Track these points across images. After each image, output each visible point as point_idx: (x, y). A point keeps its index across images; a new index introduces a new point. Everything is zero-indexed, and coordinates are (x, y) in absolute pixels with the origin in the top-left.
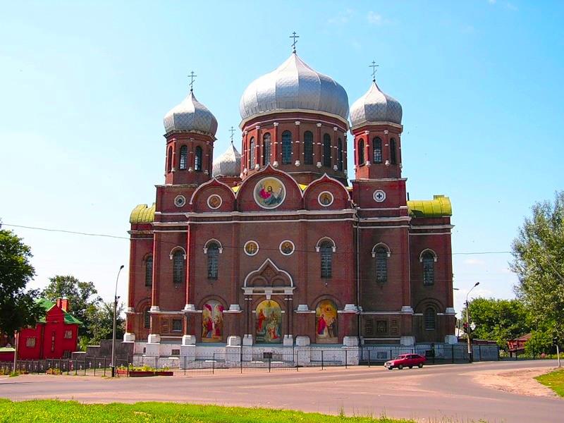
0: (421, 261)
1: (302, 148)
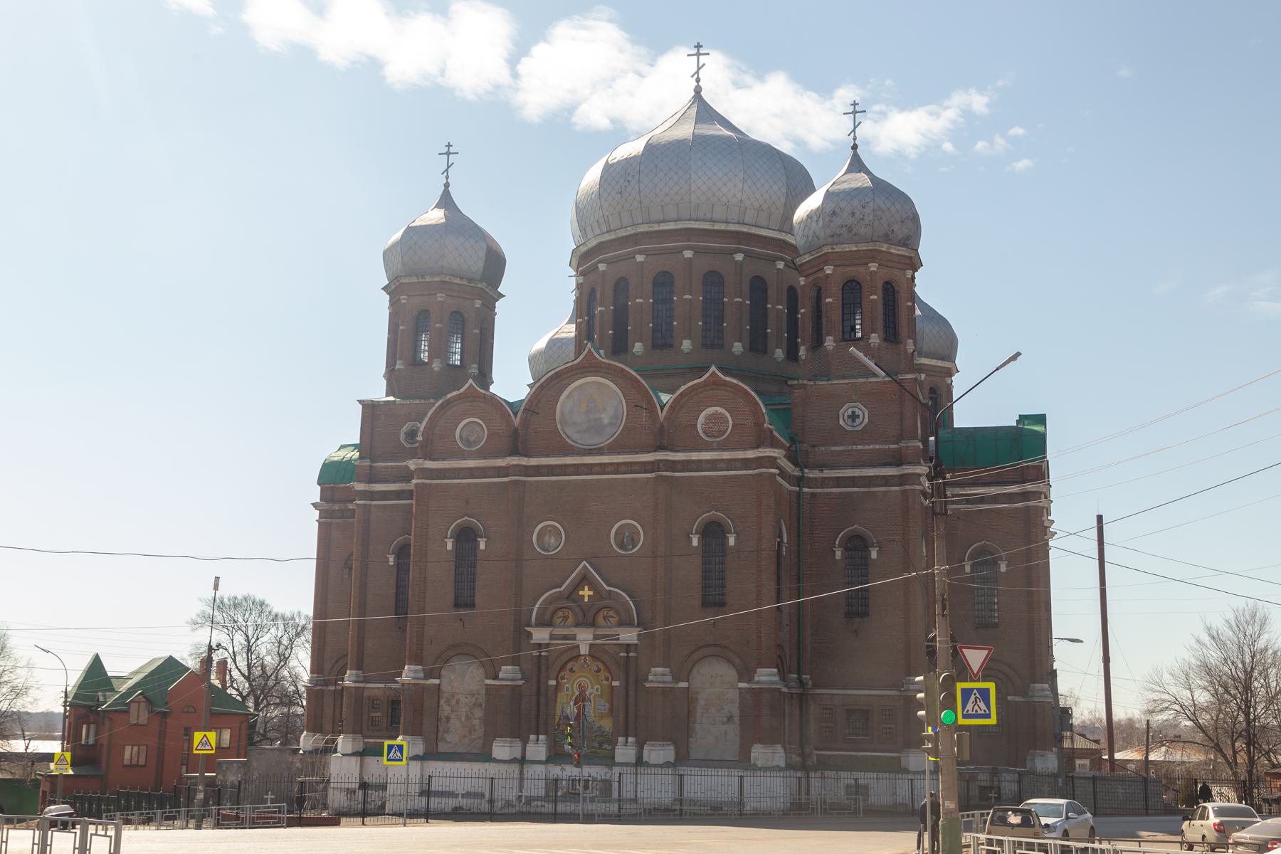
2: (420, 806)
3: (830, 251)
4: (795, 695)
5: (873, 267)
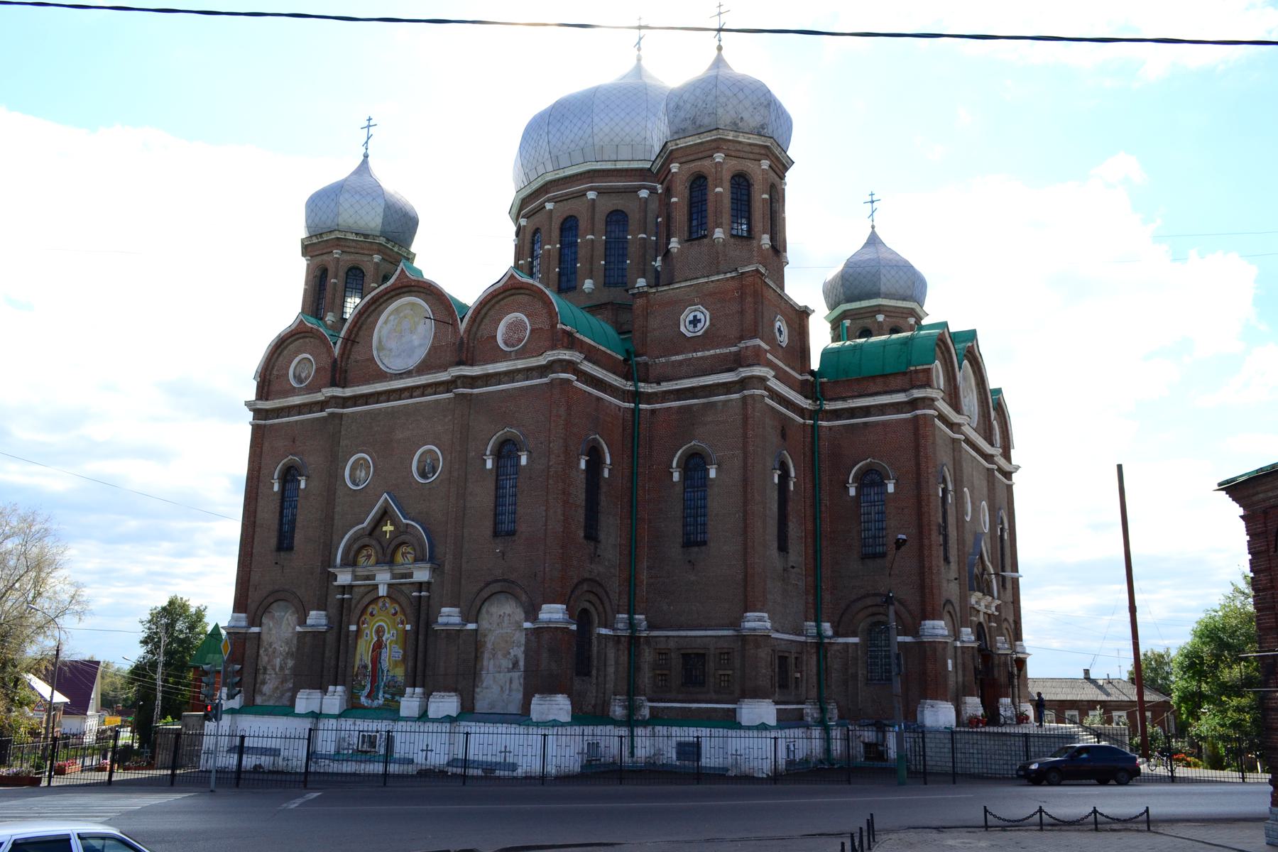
0: (852, 492)
1: (600, 250)
2: (231, 762)
3: (674, 147)
4: (623, 639)
5: (719, 157)
